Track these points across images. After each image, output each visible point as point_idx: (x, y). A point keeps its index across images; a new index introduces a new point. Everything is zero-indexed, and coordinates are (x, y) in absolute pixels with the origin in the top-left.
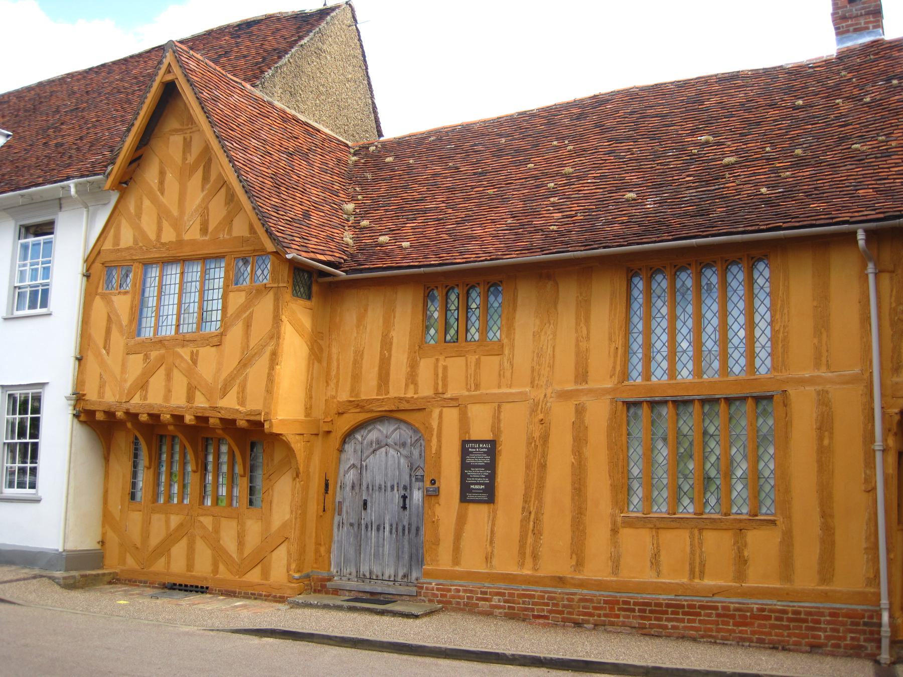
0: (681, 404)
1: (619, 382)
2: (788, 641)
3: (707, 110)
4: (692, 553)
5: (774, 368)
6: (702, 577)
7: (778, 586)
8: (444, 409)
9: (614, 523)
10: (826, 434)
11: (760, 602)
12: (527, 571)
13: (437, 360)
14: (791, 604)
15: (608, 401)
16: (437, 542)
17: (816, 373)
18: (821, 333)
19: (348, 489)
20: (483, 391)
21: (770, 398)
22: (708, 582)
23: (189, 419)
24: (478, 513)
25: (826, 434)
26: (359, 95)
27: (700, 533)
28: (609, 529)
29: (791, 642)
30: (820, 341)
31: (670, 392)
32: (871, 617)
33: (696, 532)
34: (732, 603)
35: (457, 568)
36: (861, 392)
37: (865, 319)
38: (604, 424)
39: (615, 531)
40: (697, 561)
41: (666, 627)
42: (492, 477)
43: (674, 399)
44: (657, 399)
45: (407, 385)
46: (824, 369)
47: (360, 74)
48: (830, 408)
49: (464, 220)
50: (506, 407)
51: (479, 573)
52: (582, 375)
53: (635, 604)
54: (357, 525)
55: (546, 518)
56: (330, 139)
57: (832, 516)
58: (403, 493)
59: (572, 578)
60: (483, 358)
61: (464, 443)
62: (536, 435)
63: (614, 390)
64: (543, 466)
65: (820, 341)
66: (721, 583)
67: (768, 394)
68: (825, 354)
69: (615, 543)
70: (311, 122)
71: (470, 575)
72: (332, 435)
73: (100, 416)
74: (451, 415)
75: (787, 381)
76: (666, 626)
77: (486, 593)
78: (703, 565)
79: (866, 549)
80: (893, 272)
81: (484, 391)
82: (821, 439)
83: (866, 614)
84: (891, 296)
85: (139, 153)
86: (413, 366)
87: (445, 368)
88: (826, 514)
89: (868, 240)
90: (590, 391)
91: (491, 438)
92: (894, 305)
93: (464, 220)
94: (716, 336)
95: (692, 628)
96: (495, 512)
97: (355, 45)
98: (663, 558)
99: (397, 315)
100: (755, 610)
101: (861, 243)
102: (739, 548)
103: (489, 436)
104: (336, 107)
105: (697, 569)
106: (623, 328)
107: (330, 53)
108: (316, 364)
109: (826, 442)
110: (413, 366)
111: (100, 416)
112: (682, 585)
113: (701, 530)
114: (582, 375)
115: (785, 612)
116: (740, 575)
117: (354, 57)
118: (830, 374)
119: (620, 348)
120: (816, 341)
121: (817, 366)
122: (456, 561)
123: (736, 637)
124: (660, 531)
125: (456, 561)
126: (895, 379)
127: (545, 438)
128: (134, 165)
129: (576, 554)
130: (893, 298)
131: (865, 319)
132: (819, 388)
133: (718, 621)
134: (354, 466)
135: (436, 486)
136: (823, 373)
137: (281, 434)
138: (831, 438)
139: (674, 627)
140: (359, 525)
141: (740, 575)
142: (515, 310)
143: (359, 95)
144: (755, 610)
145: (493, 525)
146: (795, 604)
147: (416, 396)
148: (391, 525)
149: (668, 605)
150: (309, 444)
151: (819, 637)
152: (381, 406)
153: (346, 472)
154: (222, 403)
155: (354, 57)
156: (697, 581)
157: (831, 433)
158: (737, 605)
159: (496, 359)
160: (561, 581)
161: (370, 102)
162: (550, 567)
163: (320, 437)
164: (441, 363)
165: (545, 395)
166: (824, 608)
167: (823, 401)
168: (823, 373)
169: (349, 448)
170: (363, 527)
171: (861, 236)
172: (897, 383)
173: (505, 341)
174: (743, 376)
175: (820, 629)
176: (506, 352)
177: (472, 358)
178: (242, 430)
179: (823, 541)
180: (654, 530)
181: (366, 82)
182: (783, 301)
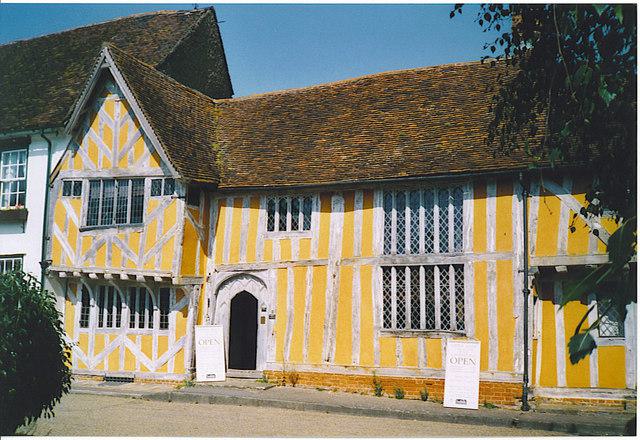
3: (434, 90)
23: (124, 277)
49: (289, 158)
73: (62, 275)
93: (289, 158)
111: (62, 275)
178: (159, 282)
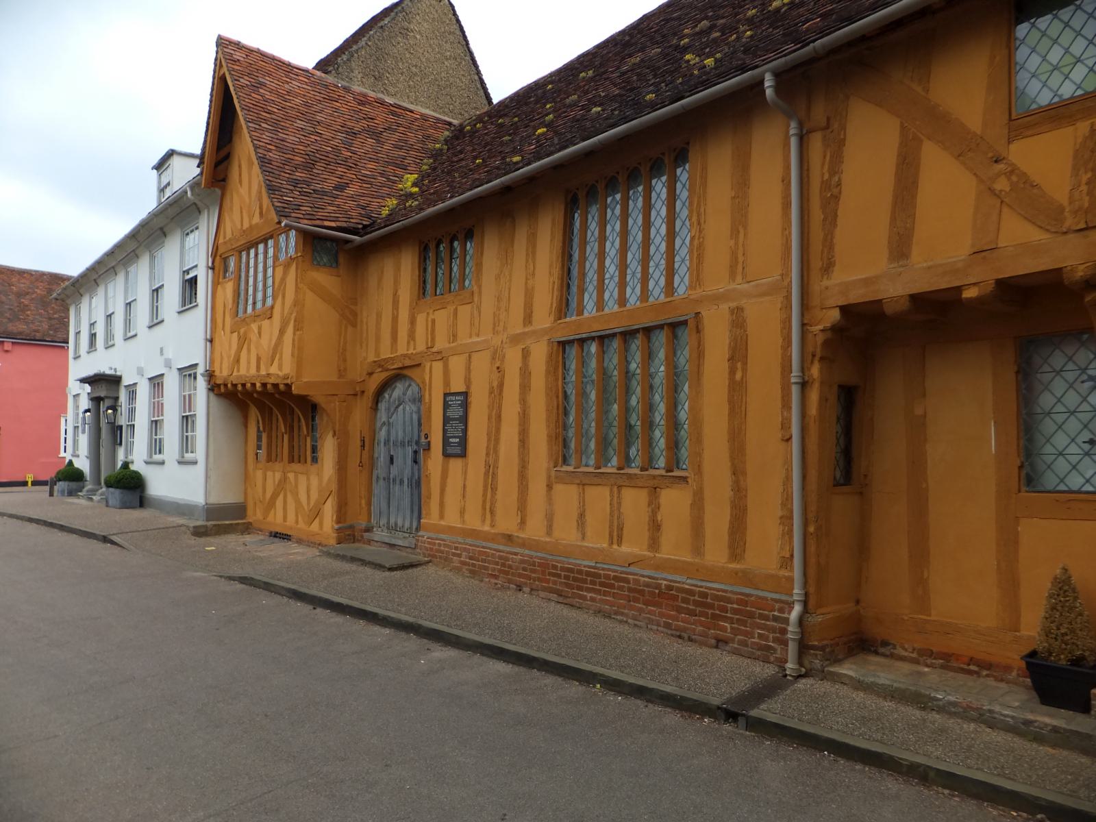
0: (603, 339)
1: (555, 321)
2: (694, 630)
4: (611, 515)
5: (691, 287)
6: (619, 543)
7: (689, 559)
8: (434, 363)
9: (549, 477)
10: (739, 365)
11: (670, 577)
12: (487, 528)
13: (428, 313)
14: (700, 583)
15: (546, 343)
16: (429, 497)
17: (733, 286)
18: (739, 232)
19: (382, 444)
20: (459, 342)
21: (685, 323)
22: (625, 549)
23: (282, 387)
24: (455, 465)
25: (739, 365)
26: (462, 73)
27: (619, 492)
28: (545, 484)
29: (697, 632)
30: (736, 244)
31: (596, 327)
32: (781, 610)
33: (615, 489)
34: (643, 576)
35: (443, 523)
36: (779, 306)
37: (786, 205)
38: (543, 368)
39: (549, 487)
40: (615, 524)
41: (584, 598)
42: (465, 431)
43: (598, 334)
44: (584, 336)
45: (408, 343)
46: (739, 279)
47: (460, 51)
48: (745, 331)
50: (475, 356)
51: (454, 527)
52: (528, 319)
53: (562, 569)
54: (387, 479)
55: (500, 472)
56: (425, 118)
57: (744, 473)
58: (415, 447)
59: (518, 537)
60: (460, 308)
61: (446, 395)
62: (495, 384)
63: (551, 329)
64: (499, 417)
65: (736, 244)
66: (636, 550)
67: (682, 319)
68: (741, 259)
69: (550, 500)
70: (405, 105)
71: (451, 530)
72: (366, 394)
74: (438, 367)
75: (698, 301)
76: (586, 596)
77: (456, 548)
78: (620, 529)
79: (781, 518)
80: (827, 127)
81: (460, 343)
82: (732, 372)
83: (777, 606)
84: (823, 164)
85: (223, 153)
86: (413, 322)
87: (433, 321)
88: (738, 471)
89: (778, 88)
90: (534, 332)
91: (464, 390)
92: (826, 176)
94: (639, 256)
95: (606, 602)
96: (466, 465)
97: (450, 20)
98: (589, 518)
99: (402, 274)
100: (663, 587)
101: (769, 92)
102: (653, 511)
103: (463, 389)
104: (436, 87)
105: (615, 534)
106: (560, 259)
107: (420, 33)
108: (350, 329)
109: (738, 376)
110: (413, 322)
112: (601, 550)
113: (620, 487)
114: (528, 319)
115: (691, 593)
116: (654, 544)
117: (450, 33)
118: (746, 286)
119: (556, 281)
120: (732, 243)
121: (733, 275)
122: (442, 516)
123: (645, 618)
124: (586, 487)
125: (442, 516)
126: (826, 283)
127: (501, 385)
128: (221, 167)
129: (521, 511)
130: (826, 167)
131: (786, 205)
132: (733, 305)
133: (629, 596)
134: (384, 423)
135: (428, 440)
136: (739, 286)
137: (308, 395)
138: (744, 371)
139: (592, 599)
140: (389, 479)
141: (654, 544)
142: (482, 254)
143: (462, 73)
144: (663, 587)
145: (465, 479)
146: (704, 584)
147: (414, 352)
148: (408, 479)
149: (588, 574)
150: (345, 404)
151: (724, 629)
152: (393, 364)
153: (381, 429)
154: (274, 370)
155: (450, 33)
156: (615, 546)
157: (745, 364)
158: (646, 579)
159: (468, 307)
160: (509, 538)
161: (476, 77)
162: (506, 523)
163: (358, 397)
164: (431, 317)
165: (502, 342)
166: (732, 592)
167: (738, 320)
168: (739, 286)
169: (382, 406)
170: (391, 481)
171: (769, 82)
172: (827, 288)
173: (475, 288)
174: (662, 298)
175: (725, 619)
176: (476, 299)
177: (451, 308)
179: (734, 506)
180: (581, 486)
181: (468, 58)
182: (699, 197)
